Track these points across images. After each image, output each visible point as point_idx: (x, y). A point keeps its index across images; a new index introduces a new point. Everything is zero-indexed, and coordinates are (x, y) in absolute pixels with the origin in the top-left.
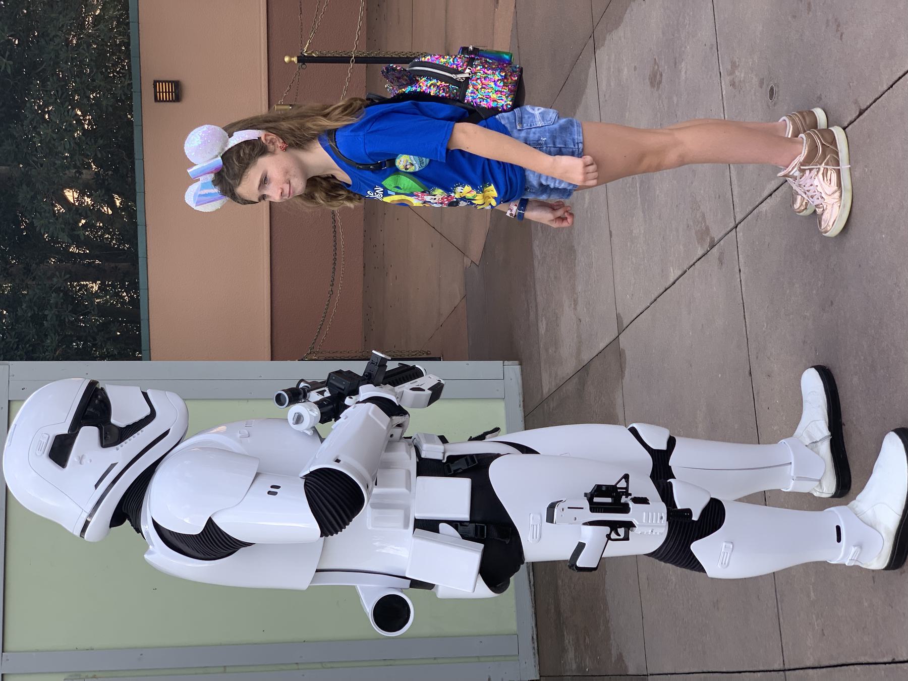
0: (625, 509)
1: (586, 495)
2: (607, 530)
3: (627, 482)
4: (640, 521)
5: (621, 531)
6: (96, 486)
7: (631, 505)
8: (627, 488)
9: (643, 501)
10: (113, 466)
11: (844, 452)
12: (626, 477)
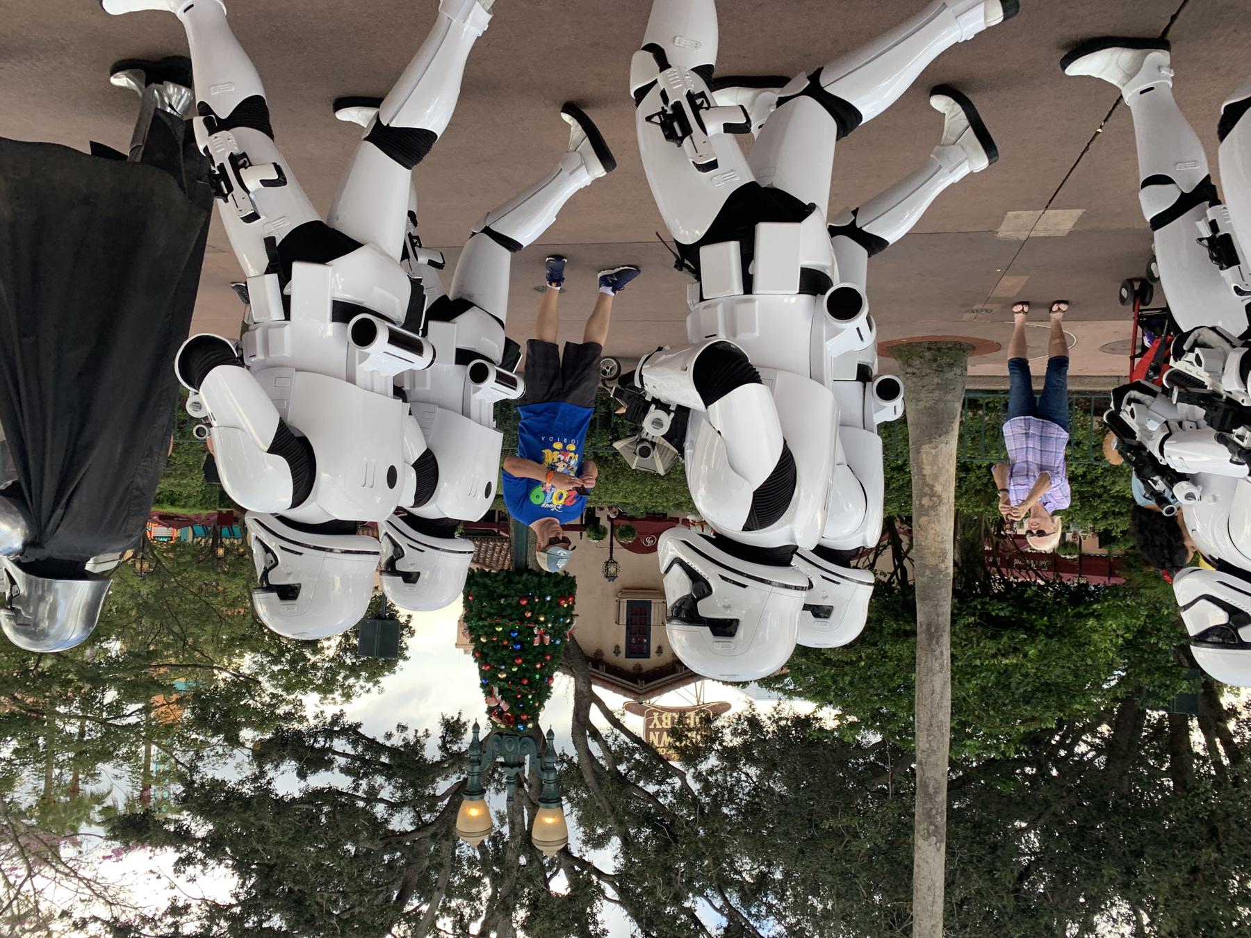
0: (677, 106)
1: (679, 146)
2: (702, 112)
3: (652, 116)
4: (682, 88)
5: (698, 101)
6: (744, 586)
7: (671, 103)
8: (658, 114)
9: (664, 95)
10: (723, 578)
11: (57, 492)
12: (649, 119)
